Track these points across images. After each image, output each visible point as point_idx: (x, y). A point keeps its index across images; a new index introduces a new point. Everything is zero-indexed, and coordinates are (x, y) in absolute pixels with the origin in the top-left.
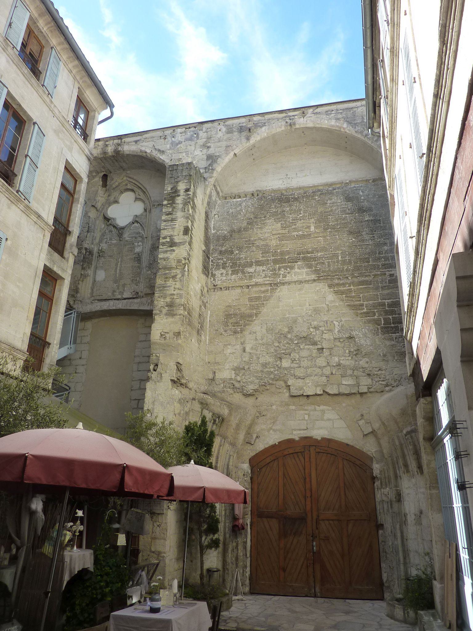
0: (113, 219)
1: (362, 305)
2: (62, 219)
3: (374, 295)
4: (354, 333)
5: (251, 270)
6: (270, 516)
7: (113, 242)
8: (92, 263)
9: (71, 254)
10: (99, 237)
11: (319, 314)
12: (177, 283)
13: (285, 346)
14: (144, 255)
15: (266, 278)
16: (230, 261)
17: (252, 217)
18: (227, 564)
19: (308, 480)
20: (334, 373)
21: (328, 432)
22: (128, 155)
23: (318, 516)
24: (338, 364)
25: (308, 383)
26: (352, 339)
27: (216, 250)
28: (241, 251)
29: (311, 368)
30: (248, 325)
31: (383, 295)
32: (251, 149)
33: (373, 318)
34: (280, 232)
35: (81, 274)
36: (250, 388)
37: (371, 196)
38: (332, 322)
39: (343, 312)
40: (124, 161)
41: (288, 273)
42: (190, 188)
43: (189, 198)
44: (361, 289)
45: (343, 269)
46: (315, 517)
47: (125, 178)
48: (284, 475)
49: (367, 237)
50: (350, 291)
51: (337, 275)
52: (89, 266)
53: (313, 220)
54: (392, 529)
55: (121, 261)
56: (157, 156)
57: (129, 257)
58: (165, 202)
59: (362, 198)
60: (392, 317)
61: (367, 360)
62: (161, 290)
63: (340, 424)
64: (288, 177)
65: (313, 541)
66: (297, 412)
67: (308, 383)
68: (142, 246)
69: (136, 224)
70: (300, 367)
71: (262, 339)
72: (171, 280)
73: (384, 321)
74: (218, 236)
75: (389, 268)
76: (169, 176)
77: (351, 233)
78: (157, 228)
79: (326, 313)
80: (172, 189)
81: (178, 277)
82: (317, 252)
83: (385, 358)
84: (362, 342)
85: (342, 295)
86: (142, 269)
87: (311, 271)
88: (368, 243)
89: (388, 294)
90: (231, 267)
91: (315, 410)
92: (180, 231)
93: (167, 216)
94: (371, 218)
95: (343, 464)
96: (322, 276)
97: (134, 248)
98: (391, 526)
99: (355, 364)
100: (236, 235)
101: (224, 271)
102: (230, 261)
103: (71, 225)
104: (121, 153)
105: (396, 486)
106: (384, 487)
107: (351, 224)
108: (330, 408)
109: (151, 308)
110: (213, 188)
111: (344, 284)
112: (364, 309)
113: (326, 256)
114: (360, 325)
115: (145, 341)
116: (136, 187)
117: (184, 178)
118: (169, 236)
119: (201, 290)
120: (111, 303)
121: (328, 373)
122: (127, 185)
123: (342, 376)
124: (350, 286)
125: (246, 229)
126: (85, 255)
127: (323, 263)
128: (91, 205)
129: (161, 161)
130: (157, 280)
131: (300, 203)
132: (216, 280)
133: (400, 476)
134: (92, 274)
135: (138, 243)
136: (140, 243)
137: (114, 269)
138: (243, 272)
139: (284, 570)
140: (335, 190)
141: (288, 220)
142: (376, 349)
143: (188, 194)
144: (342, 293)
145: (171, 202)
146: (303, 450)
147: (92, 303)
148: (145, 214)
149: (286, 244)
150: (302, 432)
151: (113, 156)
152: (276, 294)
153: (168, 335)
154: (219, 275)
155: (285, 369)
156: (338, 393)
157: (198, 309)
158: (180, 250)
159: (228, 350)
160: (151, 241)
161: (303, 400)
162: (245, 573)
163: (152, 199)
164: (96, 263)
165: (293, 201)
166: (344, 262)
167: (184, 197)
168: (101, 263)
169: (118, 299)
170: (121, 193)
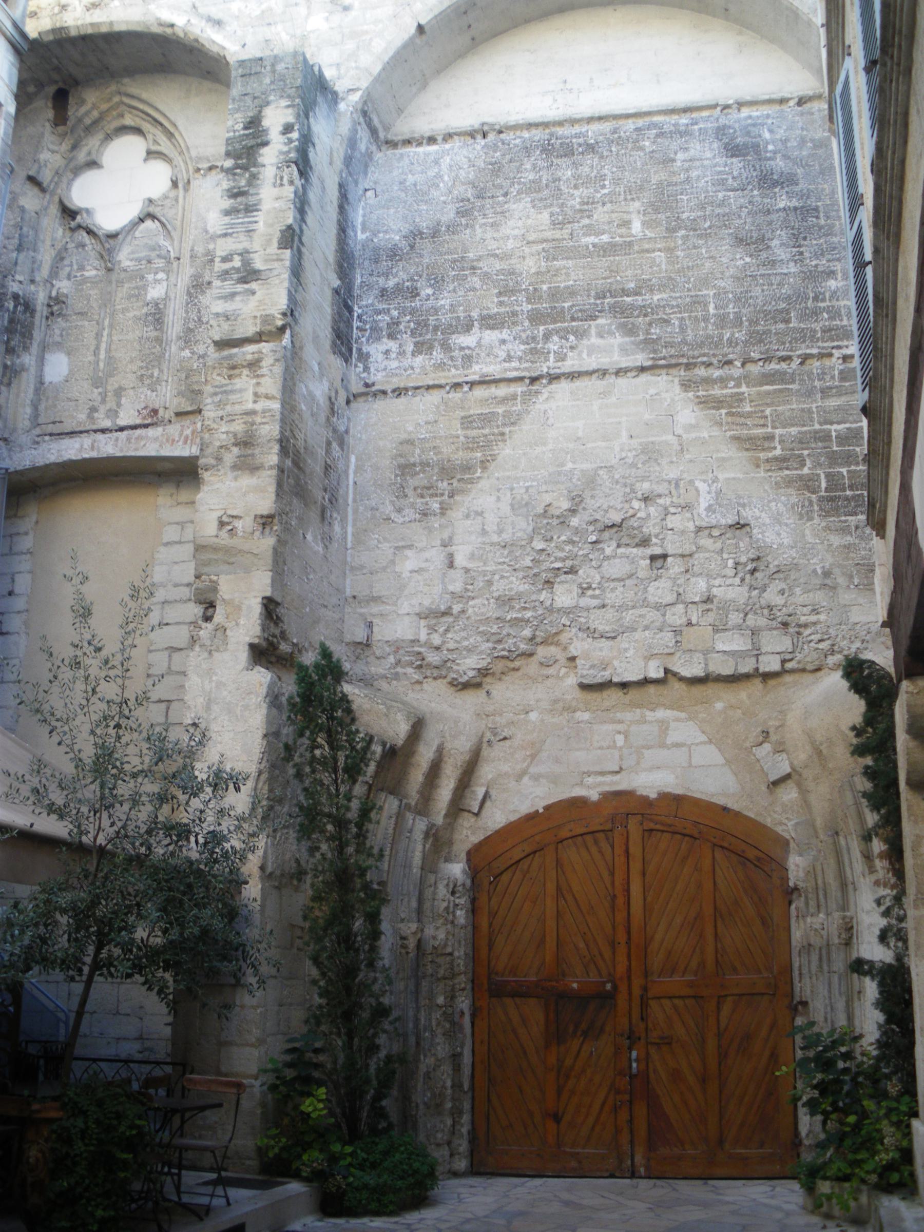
0: (88, 211)
1: (771, 438)
3: (803, 410)
4: (748, 514)
5: (467, 340)
6: (520, 993)
8: (32, 335)
10: (49, 262)
11: (656, 460)
12: (262, 380)
13: (563, 550)
15: (510, 361)
16: (408, 318)
17: (469, 196)
18: (413, 1105)
19: (620, 900)
20: (694, 622)
21: (677, 777)
23: (645, 989)
24: (705, 598)
25: (626, 650)
26: (744, 530)
27: (370, 287)
28: (439, 289)
29: (633, 607)
30: (462, 491)
31: (825, 412)
32: (465, 13)
33: (799, 472)
34: (549, 235)
36: (469, 665)
37: (793, 143)
38: (691, 482)
39: (719, 455)
41: (572, 348)
44: (768, 393)
45: (721, 339)
46: (637, 992)
48: (558, 888)
49: (782, 254)
50: (739, 398)
51: (704, 355)
52: (24, 343)
53: (637, 204)
54: (826, 1013)
55: (111, 326)
56: (204, 35)
57: (130, 315)
59: (770, 147)
60: (848, 472)
61: (783, 585)
63: (710, 755)
64: (568, 86)
65: (630, 1049)
66: (595, 727)
67: (626, 650)
68: (165, 284)
69: (149, 223)
70: (604, 606)
71: (500, 532)
72: (246, 372)
73: (828, 481)
74: (376, 250)
75: (842, 340)
77: (740, 241)
78: (207, 232)
79: (675, 459)
81: (263, 364)
82: (652, 290)
83: (828, 581)
84: (770, 537)
85: (718, 408)
87: (633, 343)
88: (785, 271)
89: (838, 409)
90: (413, 334)
91: (643, 721)
94: (795, 203)
95: (714, 857)
96: (664, 358)
97: (144, 288)
98: (826, 1006)
99: (750, 597)
100: (426, 246)
101: (393, 345)
102: (408, 318)
105: (844, 907)
106: (812, 910)
107: (740, 217)
108: (683, 715)
110: (362, 120)
111: (723, 381)
112: (775, 448)
113: (674, 303)
114: (765, 491)
115: (180, 542)
118: (240, 254)
119: (330, 399)
120: (87, 441)
121: (679, 622)
123: (716, 630)
124: (738, 385)
125: (452, 228)
126: (14, 312)
127: (667, 322)
131: (602, 157)
132: (372, 370)
133: (853, 883)
134: (33, 363)
135: (156, 273)
136: (161, 275)
137: (92, 348)
138: (446, 347)
139: (557, 1118)
140: (696, 124)
141: (569, 204)
142: (805, 555)
144: (718, 403)
146: (608, 826)
148: (172, 194)
149: (565, 267)
150: (608, 778)
152: (537, 406)
153: (239, 524)
154: (380, 357)
155: (567, 611)
156: (702, 674)
157: (321, 452)
159: (407, 563)
160: (192, 266)
161: (613, 696)
162: (457, 1127)
163: (194, 153)
164: (42, 335)
165: (582, 153)
166: (722, 321)
169: (103, 431)
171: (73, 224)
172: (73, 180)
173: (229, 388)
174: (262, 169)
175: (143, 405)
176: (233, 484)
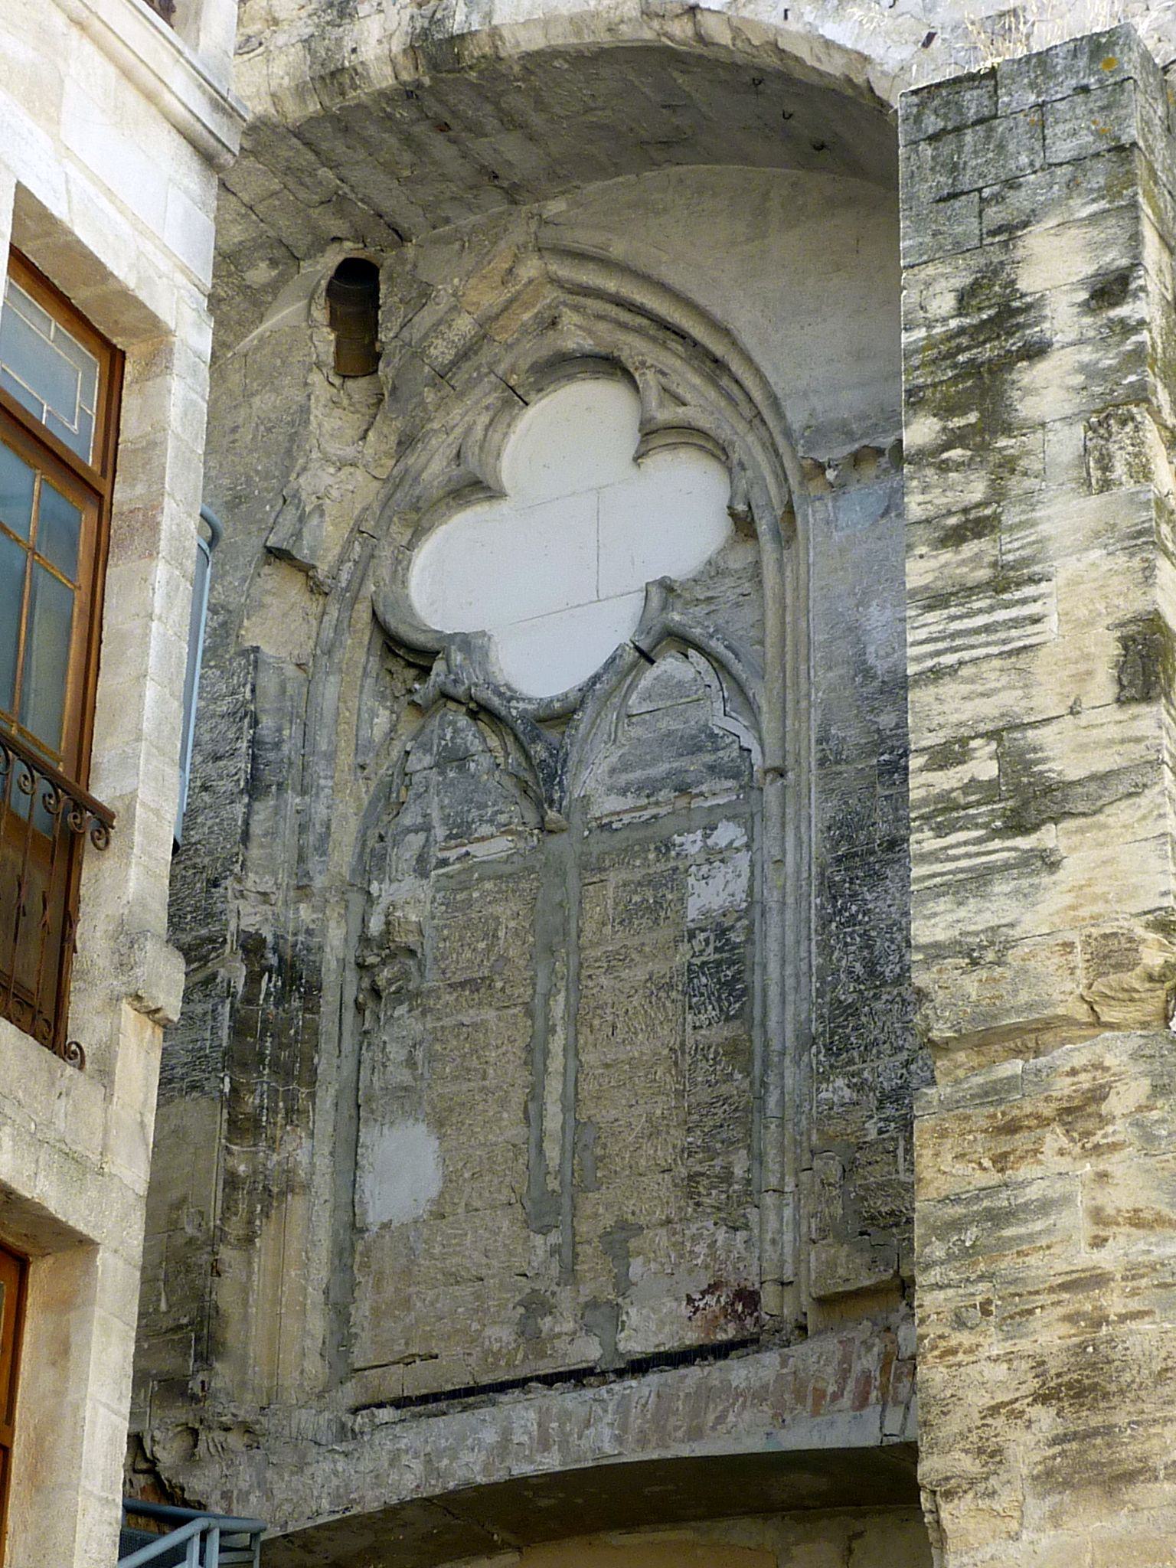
0: (465, 642)
2: (23, 704)
7: (479, 851)
8: (314, 1070)
9: (126, 1009)
10: (353, 825)
12: (1113, 1163)
14: (774, 931)
22: (537, 61)
35: (232, 1182)
40: (510, 122)
42: (1136, 264)
43: (1138, 356)
47: (530, 269)
52: (291, 1097)
55: (575, 1019)
56: (793, 26)
58: (921, 431)
62: (969, 1253)
68: (743, 860)
69: (670, 665)
72: (1054, 1138)
76: (925, 190)
78: (867, 673)
80: (965, 299)
81: (1114, 1105)
86: (766, 1064)
92: (1089, 673)
93: (947, 556)
97: (675, 879)
103: (105, 750)
104: (473, 51)
109: (893, 1425)
116: (638, 331)
117: (1072, 185)
118: (994, 735)
122: (554, 323)
126: (250, 999)
128: (254, 546)
129: (834, 66)
130: (925, 1158)
134: (323, 1163)
136: (727, 833)
137: (518, 1096)
143: (1122, 321)
145: (973, 417)
147: (344, 1432)
148: (740, 559)
151: (410, 94)
158: (1106, 853)
160: (827, 792)
163: (796, 417)
164: (349, 1066)
167: (1087, 355)
168: (397, 1052)
169: (578, 1377)
170: (506, 403)
171: (424, 691)
172: (411, 546)
173: (1002, 1201)
174: (1032, 440)
175: (705, 1280)
176: (1047, 1539)
